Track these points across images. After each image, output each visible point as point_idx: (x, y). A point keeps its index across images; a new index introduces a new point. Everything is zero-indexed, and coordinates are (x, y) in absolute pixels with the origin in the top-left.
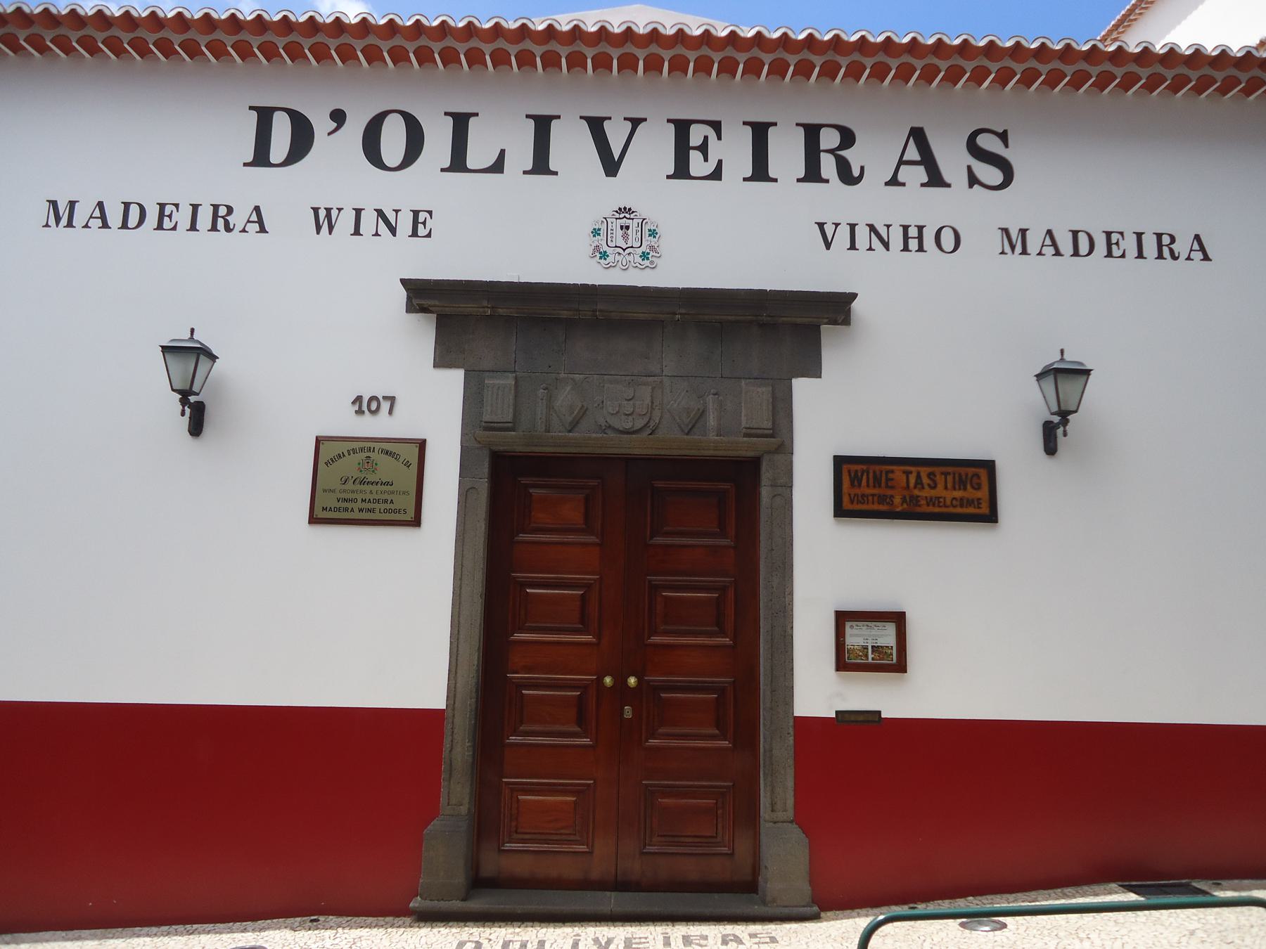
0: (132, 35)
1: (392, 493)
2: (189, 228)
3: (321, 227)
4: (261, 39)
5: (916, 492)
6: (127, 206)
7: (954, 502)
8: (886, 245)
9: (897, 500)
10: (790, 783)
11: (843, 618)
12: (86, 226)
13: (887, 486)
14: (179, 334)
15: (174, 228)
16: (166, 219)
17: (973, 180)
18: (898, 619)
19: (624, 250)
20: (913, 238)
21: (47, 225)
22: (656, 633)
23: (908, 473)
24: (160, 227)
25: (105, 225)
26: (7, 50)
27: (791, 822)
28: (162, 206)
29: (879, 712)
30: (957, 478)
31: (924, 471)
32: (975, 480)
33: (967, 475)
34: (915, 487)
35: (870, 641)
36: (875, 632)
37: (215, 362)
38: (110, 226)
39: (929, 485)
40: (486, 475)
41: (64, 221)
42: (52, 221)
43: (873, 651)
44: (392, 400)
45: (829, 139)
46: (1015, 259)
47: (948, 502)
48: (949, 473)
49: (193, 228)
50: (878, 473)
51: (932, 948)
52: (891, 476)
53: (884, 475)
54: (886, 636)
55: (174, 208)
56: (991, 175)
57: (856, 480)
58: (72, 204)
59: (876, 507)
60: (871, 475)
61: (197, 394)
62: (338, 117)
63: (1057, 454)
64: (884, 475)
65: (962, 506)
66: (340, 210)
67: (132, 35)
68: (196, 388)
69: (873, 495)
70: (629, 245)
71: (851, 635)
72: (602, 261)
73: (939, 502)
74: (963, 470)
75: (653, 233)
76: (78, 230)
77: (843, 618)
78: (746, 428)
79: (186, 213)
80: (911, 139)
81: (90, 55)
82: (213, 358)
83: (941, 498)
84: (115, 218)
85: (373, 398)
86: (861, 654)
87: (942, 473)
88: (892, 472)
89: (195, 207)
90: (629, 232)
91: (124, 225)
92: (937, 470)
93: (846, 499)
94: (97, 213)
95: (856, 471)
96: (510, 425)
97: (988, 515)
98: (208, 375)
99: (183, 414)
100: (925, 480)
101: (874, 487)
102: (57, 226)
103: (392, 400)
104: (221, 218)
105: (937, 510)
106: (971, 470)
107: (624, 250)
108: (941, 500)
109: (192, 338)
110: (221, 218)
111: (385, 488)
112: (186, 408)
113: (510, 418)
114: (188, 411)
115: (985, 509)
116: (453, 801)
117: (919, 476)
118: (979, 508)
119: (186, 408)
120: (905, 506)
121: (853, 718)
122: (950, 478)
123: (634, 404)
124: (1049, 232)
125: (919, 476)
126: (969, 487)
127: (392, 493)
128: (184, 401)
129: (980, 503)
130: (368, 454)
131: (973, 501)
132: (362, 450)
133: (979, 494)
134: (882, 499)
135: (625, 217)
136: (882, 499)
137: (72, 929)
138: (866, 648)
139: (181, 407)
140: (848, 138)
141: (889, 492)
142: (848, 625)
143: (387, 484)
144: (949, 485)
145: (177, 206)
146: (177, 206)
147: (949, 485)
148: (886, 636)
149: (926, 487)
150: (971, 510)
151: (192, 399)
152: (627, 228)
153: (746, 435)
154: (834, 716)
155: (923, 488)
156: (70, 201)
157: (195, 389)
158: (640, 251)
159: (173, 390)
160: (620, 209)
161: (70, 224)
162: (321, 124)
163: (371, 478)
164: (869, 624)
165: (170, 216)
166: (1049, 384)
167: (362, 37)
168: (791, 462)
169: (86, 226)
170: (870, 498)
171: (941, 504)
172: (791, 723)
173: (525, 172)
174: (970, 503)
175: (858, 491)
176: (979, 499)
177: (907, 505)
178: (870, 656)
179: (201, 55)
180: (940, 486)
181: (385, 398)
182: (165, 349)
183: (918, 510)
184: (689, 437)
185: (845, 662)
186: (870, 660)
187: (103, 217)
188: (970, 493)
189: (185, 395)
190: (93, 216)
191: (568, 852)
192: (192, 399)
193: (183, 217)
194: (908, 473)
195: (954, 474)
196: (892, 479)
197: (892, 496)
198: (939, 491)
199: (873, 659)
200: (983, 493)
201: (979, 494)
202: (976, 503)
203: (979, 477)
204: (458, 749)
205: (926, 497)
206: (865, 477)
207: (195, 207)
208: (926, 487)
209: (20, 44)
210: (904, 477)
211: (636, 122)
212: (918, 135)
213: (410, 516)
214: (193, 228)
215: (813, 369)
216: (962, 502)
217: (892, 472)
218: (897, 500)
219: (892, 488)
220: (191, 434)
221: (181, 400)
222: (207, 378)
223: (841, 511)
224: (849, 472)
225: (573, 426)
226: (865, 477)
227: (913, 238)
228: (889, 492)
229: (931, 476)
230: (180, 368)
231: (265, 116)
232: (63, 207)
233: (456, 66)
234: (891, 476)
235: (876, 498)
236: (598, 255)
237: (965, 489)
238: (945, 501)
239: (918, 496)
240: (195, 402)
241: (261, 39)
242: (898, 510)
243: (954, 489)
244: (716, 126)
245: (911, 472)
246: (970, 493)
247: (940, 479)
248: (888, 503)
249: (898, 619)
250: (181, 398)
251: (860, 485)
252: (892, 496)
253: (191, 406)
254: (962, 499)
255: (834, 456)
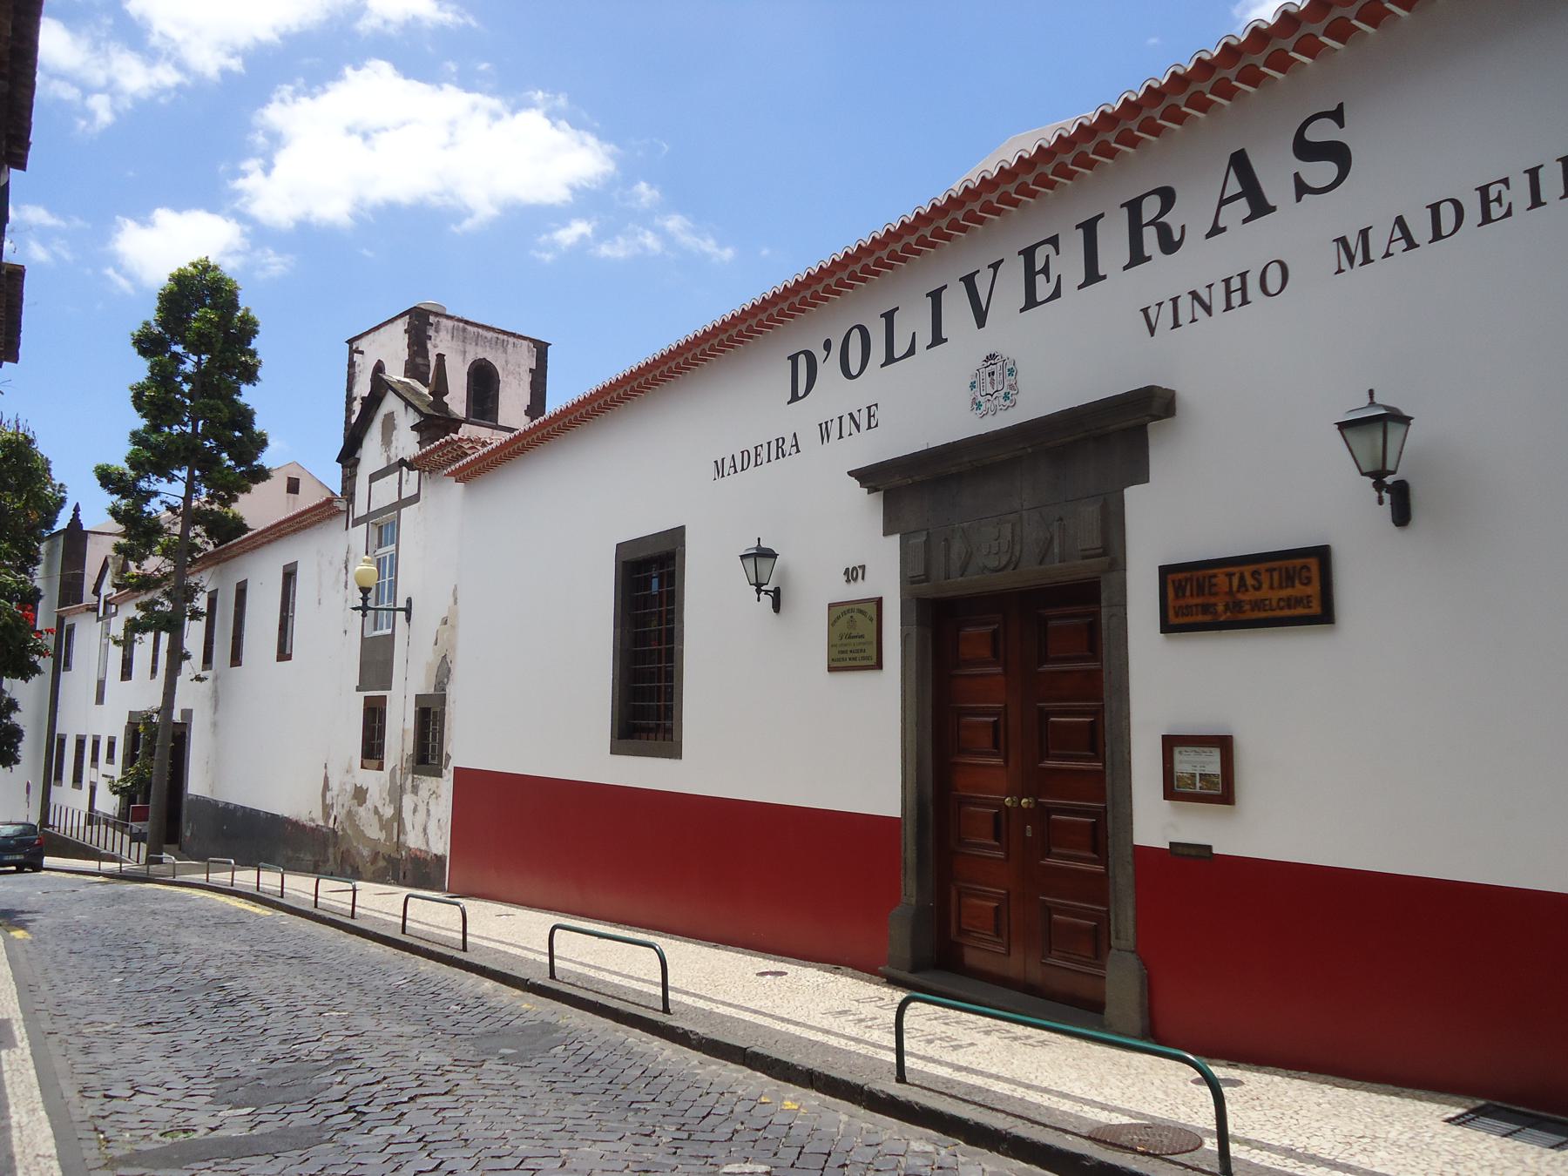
0: (963, 211)
1: (864, 644)
2: (1529, 205)
3: (1155, 328)
4: (1093, 144)
5: (1240, 596)
6: (1435, 209)
7: (1282, 604)
8: (1208, 309)
9: (1220, 608)
10: (1131, 913)
11: (1171, 743)
12: (1388, 255)
13: (1211, 594)
14: (1353, 405)
15: (1509, 213)
16: (1494, 206)
17: (1302, 189)
18: (1224, 744)
19: (992, 396)
20: (1236, 291)
21: (1340, 271)
22: (1048, 757)
23: (1230, 575)
24: (1487, 218)
25: (1411, 245)
26: (960, 234)
27: (1133, 952)
28: (1484, 191)
29: (1210, 847)
30: (1284, 574)
31: (1247, 570)
32: (1305, 573)
33: (1294, 568)
34: (1238, 591)
35: (1198, 768)
36: (1203, 758)
37: (1409, 425)
38: (1417, 243)
39: (1253, 586)
40: (915, 622)
41: (1359, 258)
42: (1345, 264)
43: (1200, 780)
44: (863, 567)
45: (1151, 208)
46: (1359, 273)
47: (1274, 603)
48: (1275, 569)
49: (1536, 202)
50: (1201, 579)
51: (1425, 1175)
52: (1214, 581)
53: (1207, 580)
54: (1210, 762)
55: (1502, 186)
56: (1327, 170)
57: (1180, 589)
58: (1364, 234)
59: (1200, 618)
60: (1195, 583)
61: (1393, 473)
62: (827, 345)
63: (1411, 522)
64: (1207, 580)
65: (1289, 607)
66: (832, 421)
67: (963, 211)
68: (1390, 466)
69: (1196, 605)
70: (995, 389)
71: (1181, 762)
72: (979, 412)
73: (1265, 605)
74: (1289, 563)
75: (1011, 372)
76: (1379, 265)
77: (1171, 743)
78: (1082, 550)
79: (1521, 185)
80: (1232, 170)
81: (1373, 27)
82: (1406, 420)
83: (1266, 600)
84: (1421, 228)
85: (854, 568)
86: (1189, 782)
87: (1267, 571)
88: (1215, 576)
89: (1533, 173)
90: (995, 377)
91: (1437, 235)
92: (1262, 567)
93: (1171, 613)
94: (1398, 234)
95: (1180, 581)
96: (923, 577)
97: (1324, 615)
98: (1403, 445)
99: (1381, 502)
100: (1250, 581)
101: (1198, 595)
102: (1352, 268)
103: (863, 567)
104: (779, 449)
105: (1263, 615)
106: (1299, 562)
107: (992, 396)
108: (1267, 602)
109: (1372, 403)
110: (779, 449)
111: (857, 640)
112: (1384, 494)
113: (1098, 543)
114: (1387, 497)
115: (1316, 608)
116: (908, 894)
117: (1242, 578)
118: (1310, 607)
119: (1384, 494)
120: (1229, 614)
121: (1186, 851)
122: (1276, 575)
123: (999, 543)
124: (1400, 221)
125: (1242, 578)
126: (1297, 582)
127: (864, 644)
128: (1379, 486)
129: (1311, 602)
130: (850, 615)
131: (1302, 599)
132: (844, 613)
133: (1309, 590)
134: (1206, 609)
135: (991, 364)
136: (1206, 609)
137: (809, 960)
138: (1193, 775)
139: (1377, 494)
140: (1167, 197)
141: (1213, 600)
142: (1177, 750)
143: (862, 636)
144: (1276, 584)
145: (1505, 181)
146: (1505, 181)
147: (1276, 584)
148: (1210, 762)
149: (1250, 588)
150: (1300, 611)
151: (1389, 480)
152: (993, 373)
153: (1085, 557)
154: (1168, 848)
155: (1247, 590)
156: (1361, 231)
157: (1390, 467)
158: (1002, 393)
159: (1363, 474)
160: (987, 358)
161: (1367, 260)
162: (820, 354)
163: (854, 634)
164: (1197, 749)
165: (1499, 199)
166: (750, 563)
167: (1183, 90)
168: (1125, 578)
169: (1388, 255)
170: (1194, 609)
171: (1267, 608)
172: (1130, 851)
173: (1245, 221)
174: (1298, 601)
175: (1182, 602)
176: (1309, 596)
177: (1231, 612)
178: (1198, 785)
179: (1265, 77)
180: (1265, 586)
181: (859, 567)
182: (1343, 426)
183: (1242, 617)
184: (1042, 567)
185: (1172, 790)
186: (1198, 790)
187: (1407, 235)
188: (1298, 590)
189: (1378, 477)
190: (1393, 239)
191: (1088, 974)
192: (1389, 480)
193: (1519, 193)
194: (1230, 575)
195: (1280, 569)
196: (1215, 585)
197: (1215, 605)
198: (1264, 593)
199: (1201, 788)
200: (1314, 589)
201: (1309, 590)
202: (1305, 602)
203: (1309, 569)
204: (909, 851)
205: (1250, 601)
206: (1188, 587)
207: (1533, 173)
208: (1250, 588)
209: (1091, 158)
210: (1227, 580)
211: (995, 266)
212: (1240, 163)
213: (873, 662)
214: (1536, 202)
215: (1140, 474)
216: (1290, 602)
217: (1215, 576)
218: (1220, 608)
219: (1216, 594)
220: (1396, 526)
221: (1375, 485)
222: (1401, 453)
223: (1167, 627)
224: (1173, 582)
225: (963, 572)
226: (1188, 587)
227: (1236, 291)
228: (1213, 600)
229: (1257, 576)
230: (1367, 443)
231: (794, 359)
232: (1353, 241)
233: (909, 259)
234: (1214, 581)
235: (1200, 608)
236: (975, 406)
237: (1293, 586)
238: (1271, 603)
239: (1241, 601)
240: (1394, 482)
241: (1093, 144)
242: (1222, 619)
243: (1281, 587)
244: (1054, 241)
245: (1233, 574)
246: (1298, 590)
247: (1265, 578)
248: (1211, 613)
249: (1224, 744)
250: (1374, 483)
251: (1184, 595)
252: (1215, 605)
253: (1390, 489)
254: (1289, 599)
255: (1160, 567)
